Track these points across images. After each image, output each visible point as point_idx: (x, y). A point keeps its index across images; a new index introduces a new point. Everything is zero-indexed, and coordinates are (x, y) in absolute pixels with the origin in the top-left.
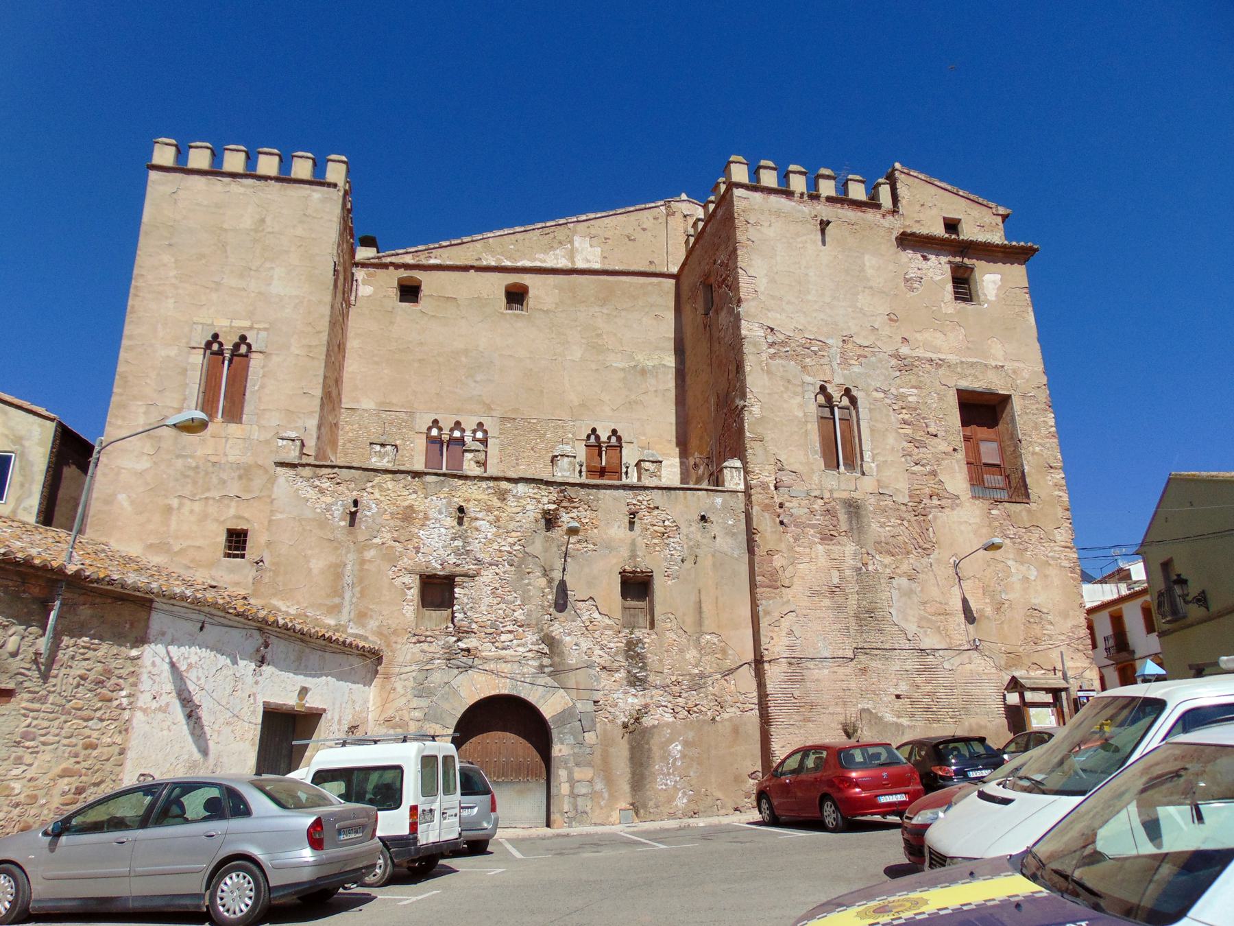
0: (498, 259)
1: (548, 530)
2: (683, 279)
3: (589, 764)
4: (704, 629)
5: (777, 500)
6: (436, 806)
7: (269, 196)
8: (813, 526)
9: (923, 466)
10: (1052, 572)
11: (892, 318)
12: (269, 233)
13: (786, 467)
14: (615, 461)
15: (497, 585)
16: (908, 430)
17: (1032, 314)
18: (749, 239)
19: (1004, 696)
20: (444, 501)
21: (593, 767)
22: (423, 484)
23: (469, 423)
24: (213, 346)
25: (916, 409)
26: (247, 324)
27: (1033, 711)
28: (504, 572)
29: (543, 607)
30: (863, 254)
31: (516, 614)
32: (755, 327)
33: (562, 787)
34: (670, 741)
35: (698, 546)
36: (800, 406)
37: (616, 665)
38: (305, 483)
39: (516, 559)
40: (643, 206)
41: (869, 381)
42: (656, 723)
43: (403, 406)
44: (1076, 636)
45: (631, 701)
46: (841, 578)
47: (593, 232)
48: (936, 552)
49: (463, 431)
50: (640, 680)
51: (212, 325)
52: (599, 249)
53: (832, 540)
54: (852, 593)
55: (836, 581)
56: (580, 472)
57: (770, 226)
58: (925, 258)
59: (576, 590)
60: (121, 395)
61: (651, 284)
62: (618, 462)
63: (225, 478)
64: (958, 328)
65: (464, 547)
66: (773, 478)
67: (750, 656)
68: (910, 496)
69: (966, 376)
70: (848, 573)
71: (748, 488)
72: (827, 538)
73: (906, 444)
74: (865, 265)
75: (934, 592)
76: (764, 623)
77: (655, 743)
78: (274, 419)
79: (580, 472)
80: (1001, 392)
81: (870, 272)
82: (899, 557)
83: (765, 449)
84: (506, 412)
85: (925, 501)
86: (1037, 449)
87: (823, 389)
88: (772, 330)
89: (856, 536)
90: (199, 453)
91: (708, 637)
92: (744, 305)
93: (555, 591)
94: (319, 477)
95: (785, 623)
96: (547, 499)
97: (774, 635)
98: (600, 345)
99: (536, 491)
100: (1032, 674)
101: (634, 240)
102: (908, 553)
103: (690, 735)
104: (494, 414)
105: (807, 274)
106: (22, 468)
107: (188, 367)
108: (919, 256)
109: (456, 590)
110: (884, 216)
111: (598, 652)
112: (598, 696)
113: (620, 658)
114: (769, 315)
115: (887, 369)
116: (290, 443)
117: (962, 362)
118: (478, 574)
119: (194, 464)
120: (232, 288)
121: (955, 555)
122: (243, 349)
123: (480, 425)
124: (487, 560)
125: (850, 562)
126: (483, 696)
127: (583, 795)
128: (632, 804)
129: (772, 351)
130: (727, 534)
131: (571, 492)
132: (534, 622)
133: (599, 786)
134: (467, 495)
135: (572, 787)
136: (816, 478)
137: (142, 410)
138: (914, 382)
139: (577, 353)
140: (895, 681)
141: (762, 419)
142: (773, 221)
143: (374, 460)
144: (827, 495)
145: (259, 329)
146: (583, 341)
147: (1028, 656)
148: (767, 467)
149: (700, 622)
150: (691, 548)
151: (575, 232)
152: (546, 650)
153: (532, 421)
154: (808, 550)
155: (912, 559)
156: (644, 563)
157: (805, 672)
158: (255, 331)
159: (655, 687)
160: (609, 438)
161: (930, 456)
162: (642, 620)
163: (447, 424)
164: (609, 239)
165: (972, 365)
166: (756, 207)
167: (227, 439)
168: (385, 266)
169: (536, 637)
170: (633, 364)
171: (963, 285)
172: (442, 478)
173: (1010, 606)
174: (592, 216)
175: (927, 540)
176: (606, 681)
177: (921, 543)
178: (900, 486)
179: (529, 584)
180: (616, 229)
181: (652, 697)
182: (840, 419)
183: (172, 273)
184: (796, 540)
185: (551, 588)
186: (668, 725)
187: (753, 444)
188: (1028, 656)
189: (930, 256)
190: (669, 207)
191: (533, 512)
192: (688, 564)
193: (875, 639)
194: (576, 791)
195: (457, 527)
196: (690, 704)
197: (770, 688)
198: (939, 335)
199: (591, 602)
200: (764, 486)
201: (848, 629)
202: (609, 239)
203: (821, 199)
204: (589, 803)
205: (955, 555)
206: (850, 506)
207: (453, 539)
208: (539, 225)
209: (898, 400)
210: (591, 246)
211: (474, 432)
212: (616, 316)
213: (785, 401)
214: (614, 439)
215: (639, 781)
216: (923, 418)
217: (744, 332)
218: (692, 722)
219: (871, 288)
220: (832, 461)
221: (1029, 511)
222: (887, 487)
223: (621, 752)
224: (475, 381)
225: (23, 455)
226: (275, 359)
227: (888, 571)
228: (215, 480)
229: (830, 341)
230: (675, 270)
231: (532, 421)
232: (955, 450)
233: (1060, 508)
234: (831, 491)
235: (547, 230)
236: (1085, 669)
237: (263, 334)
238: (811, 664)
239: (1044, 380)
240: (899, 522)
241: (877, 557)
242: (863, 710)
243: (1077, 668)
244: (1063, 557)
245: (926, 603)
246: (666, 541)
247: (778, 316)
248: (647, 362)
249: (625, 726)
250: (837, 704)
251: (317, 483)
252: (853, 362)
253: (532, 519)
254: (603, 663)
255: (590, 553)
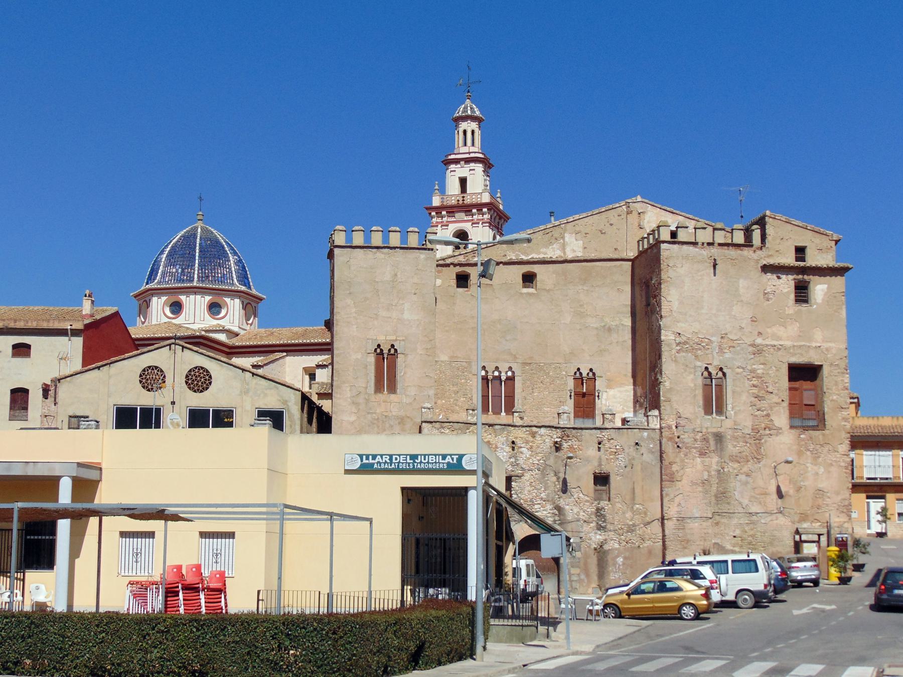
0: (517, 255)
1: (557, 451)
2: (637, 262)
3: (578, 567)
4: (635, 502)
5: (676, 434)
6: (530, 580)
7: (397, 259)
8: (695, 448)
9: (762, 411)
10: (833, 469)
11: (754, 320)
12: (400, 282)
13: (682, 416)
14: (591, 388)
15: (532, 481)
16: (755, 391)
17: (844, 313)
18: (669, 277)
19: (794, 536)
20: (505, 438)
21: (580, 568)
22: (494, 429)
23: (504, 367)
24: (379, 353)
25: (761, 378)
26: (394, 338)
27: (805, 545)
28: (536, 474)
29: (555, 491)
30: (739, 279)
31: (542, 495)
32: (669, 333)
33: (565, 576)
34: (617, 556)
35: (633, 459)
36: (692, 380)
37: (591, 520)
38: (437, 431)
39: (541, 468)
40: (611, 206)
41: (735, 362)
42: (610, 548)
43: (464, 359)
44: (842, 505)
45: (598, 537)
46: (709, 476)
47: (577, 229)
48: (764, 460)
49: (500, 372)
50: (603, 527)
51: (376, 339)
52: (581, 242)
53: (705, 455)
54: (714, 484)
55: (706, 477)
56: (570, 396)
57: (682, 267)
58: (779, 278)
59: (571, 483)
60: (337, 381)
61: (615, 266)
62: (593, 388)
63: (392, 424)
64: (795, 323)
65: (515, 462)
66: (675, 422)
67: (659, 516)
68: (752, 429)
69: (796, 354)
70: (713, 473)
71: (661, 428)
72: (702, 454)
73: (753, 399)
74: (739, 286)
75: (761, 483)
76: (665, 500)
77: (609, 558)
78: (412, 391)
79: (570, 396)
80: (816, 363)
81: (742, 291)
82: (742, 464)
83: (671, 407)
84: (525, 359)
85: (761, 432)
86: (835, 397)
87: (706, 368)
88: (679, 334)
89: (719, 454)
90: (378, 411)
91: (637, 506)
92: (664, 320)
93: (561, 483)
94: (443, 428)
95: (677, 500)
96: (556, 436)
97: (671, 506)
98: (582, 312)
99: (550, 431)
100: (814, 525)
101: (605, 233)
102: (748, 461)
103: (627, 554)
104: (517, 361)
105: (703, 297)
106: (289, 417)
107: (368, 364)
108: (775, 276)
109: (512, 483)
110: (755, 251)
111: (582, 513)
112: (582, 535)
113: (593, 516)
114: (679, 325)
115: (746, 354)
116: (428, 410)
117: (794, 346)
118: (523, 475)
119: (376, 417)
120: (384, 317)
121: (775, 462)
122: (392, 351)
123: (510, 368)
124: (528, 468)
125: (715, 467)
126: (527, 534)
127: (576, 581)
128: (598, 585)
129: (678, 348)
130: (649, 452)
131: (568, 432)
132: (551, 499)
133: (583, 577)
134: (516, 435)
135: (570, 577)
136: (699, 422)
137: (348, 389)
138: (762, 361)
139: (568, 319)
140: (733, 529)
141: (671, 389)
142: (684, 263)
143: (469, 418)
144: (704, 430)
145: (400, 340)
146: (572, 310)
147: (813, 515)
148: (672, 416)
149: (633, 499)
150: (630, 460)
151: (565, 231)
152: (557, 513)
153: (541, 364)
154: (692, 461)
155: (750, 465)
156: (605, 469)
157: (685, 525)
158: (398, 342)
159: (610, 531)
160: (588, 374)
161: (766, 405)
162: (605, 496)
163: (490, 368)
164: (588, 234)
165: (800, 346)
166: (674, 255)
167: (391, 403)
168: (448, 265)
169: (552, 506)
170: (603, 324)
171: (802, 293)
172: (503, 427)
173: (805, 489)
174: (577, 217)
175: (759, 454)
176: (586, 528)
177: (756, 456)
178: (747, 424)
179: (548, 480)
180: (593, 226)
181: (608, 536)
182: (715, 385)
183: (354, 310)
184: (686, 455)
185: (559, 482)
186: (616, 549)
187: (665, 403)
188: (813, 515)
189: (782, 276)
190: (629, 207)
191: (549, 442)
192: (629, 468)
193: (725, 508)
194: (572, 579)
195: (512, 452)
196: (628, 539)
197: (667, 532)
198: (782, 329)
199: (578, 489)
200: (670, 427)
201: (710, 503)
202: (588, 234)
203: (715, 244)
204: (578, 584)
205: (775, 462)
206: (717, 436)
207: (510, 458)
208: (542, 227)
209: (751, 372)
210: (576, 240)
211: (506, 373)
212: (592, 291)
213: (684, 378)
214: (591, 374)
215: (602, 574)
216: (765, 383)
217: (663, 338)
218: (628, 548)
219: (742, 301)
220: (708, 410)
221: (824, 435)
222: (739, 425)
223: (593, 561)
224: (506, 340)
225: (289, 411)
226: (410, 357)
227: (736, 471)
228: (387, 425)
229: (713, 339)
230: (632, 254)
231: (541, 364)
232: (783, 401)
233: (844, 432)
234: (707, 428)
235: (547, 231)
236: (845, 522)
237: (402, 343)
238: (689, 521)
239: (846, 353)
240: (745, 444)
241: (730, 464)
242: (715, 543)
243: (840, 522)
244: (841, 460)
245: (755, 488)
246: (617, 457)
247: (683, 325)
248: (612, 323)
249: (595, 549)
250: (701, 540)
251: (443, 431)
252: (726, 351)
253: (548, 447)
254: (584, 519)
255: (578, 464)
